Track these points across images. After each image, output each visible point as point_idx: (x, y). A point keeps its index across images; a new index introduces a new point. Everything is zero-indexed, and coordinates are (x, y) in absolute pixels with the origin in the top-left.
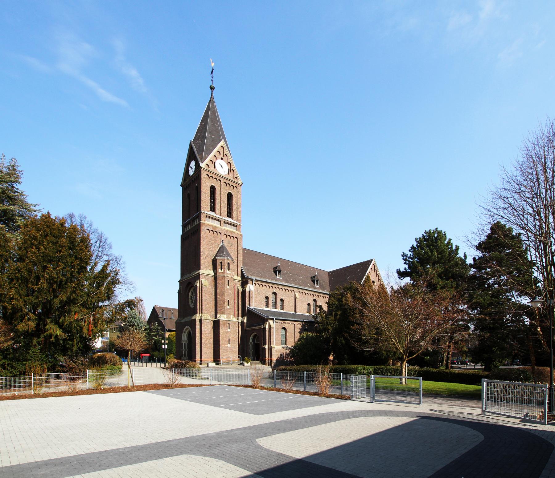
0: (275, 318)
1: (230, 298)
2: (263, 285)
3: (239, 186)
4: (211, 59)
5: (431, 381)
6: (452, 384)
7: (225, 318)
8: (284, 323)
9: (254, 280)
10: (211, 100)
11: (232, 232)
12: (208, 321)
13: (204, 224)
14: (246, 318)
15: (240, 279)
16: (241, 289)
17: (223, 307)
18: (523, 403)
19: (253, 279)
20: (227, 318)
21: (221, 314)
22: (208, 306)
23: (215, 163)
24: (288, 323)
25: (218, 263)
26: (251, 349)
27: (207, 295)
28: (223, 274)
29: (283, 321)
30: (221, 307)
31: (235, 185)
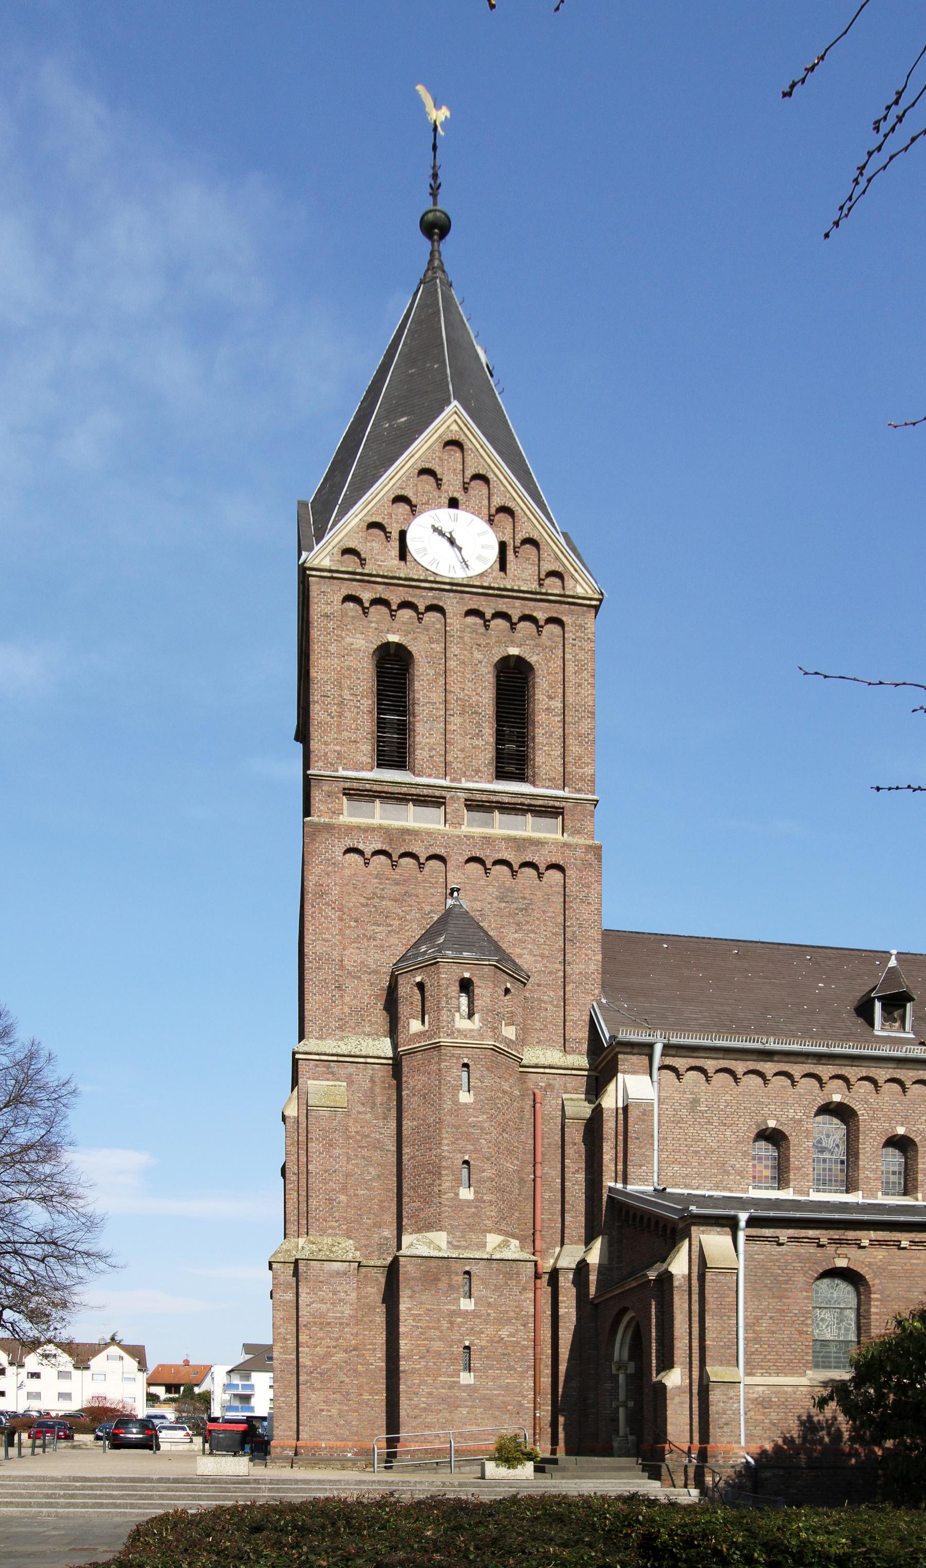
0: (743, 1217)
1: (476, 1151)
2: (797, 1076)
3: (571, 613)
4: (420, 88)
5: (603, 1456)
6: (602, 1459)
7: (440, 1250)
8: (839, 1242)
9: (658, 1049)
10: (434, 266)
11: (520, 844)
12: (336, 1266)
13: (329, 828)
14: (598, 1244)
15: (583, 1061)
16: (581, 1108)
17: (429, 1197)
18: (524, 714)
19: (651, 1046)
20: (457, 1247)
21: (419, 1231)
22: (343, 1198)
23: (403, 535)
24: (833, 1241)
25: (406, 988)
26: (622, 1396)
27: (337, 1152)
28: (430, 1038)
29: (836, 1234)
30: (420, 1196)
31: (544, 610)
